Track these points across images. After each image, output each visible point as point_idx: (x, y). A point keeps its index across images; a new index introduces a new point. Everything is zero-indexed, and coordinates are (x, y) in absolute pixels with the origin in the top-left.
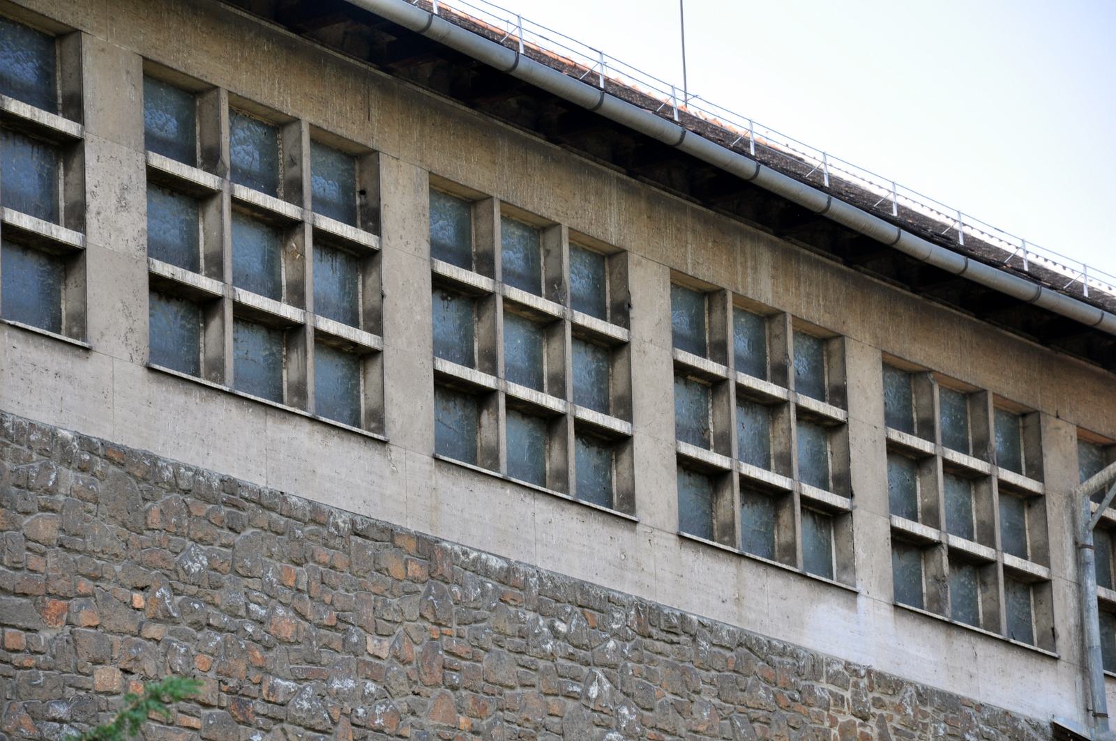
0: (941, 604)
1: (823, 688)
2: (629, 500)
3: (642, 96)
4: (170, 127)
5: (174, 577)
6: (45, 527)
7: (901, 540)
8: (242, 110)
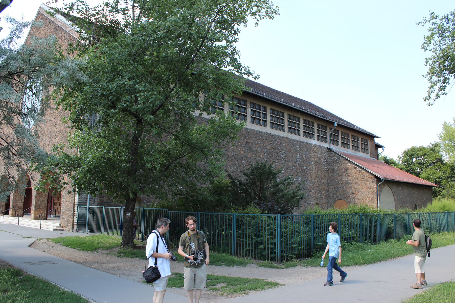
0: (66, 66)
1: (312, 146)
2: (300, 134)
3: (65, 17)
4: (271, 112)
5: (272, 141)
6: (264, 138)
7: (318, 136)
8: (276, 111)
